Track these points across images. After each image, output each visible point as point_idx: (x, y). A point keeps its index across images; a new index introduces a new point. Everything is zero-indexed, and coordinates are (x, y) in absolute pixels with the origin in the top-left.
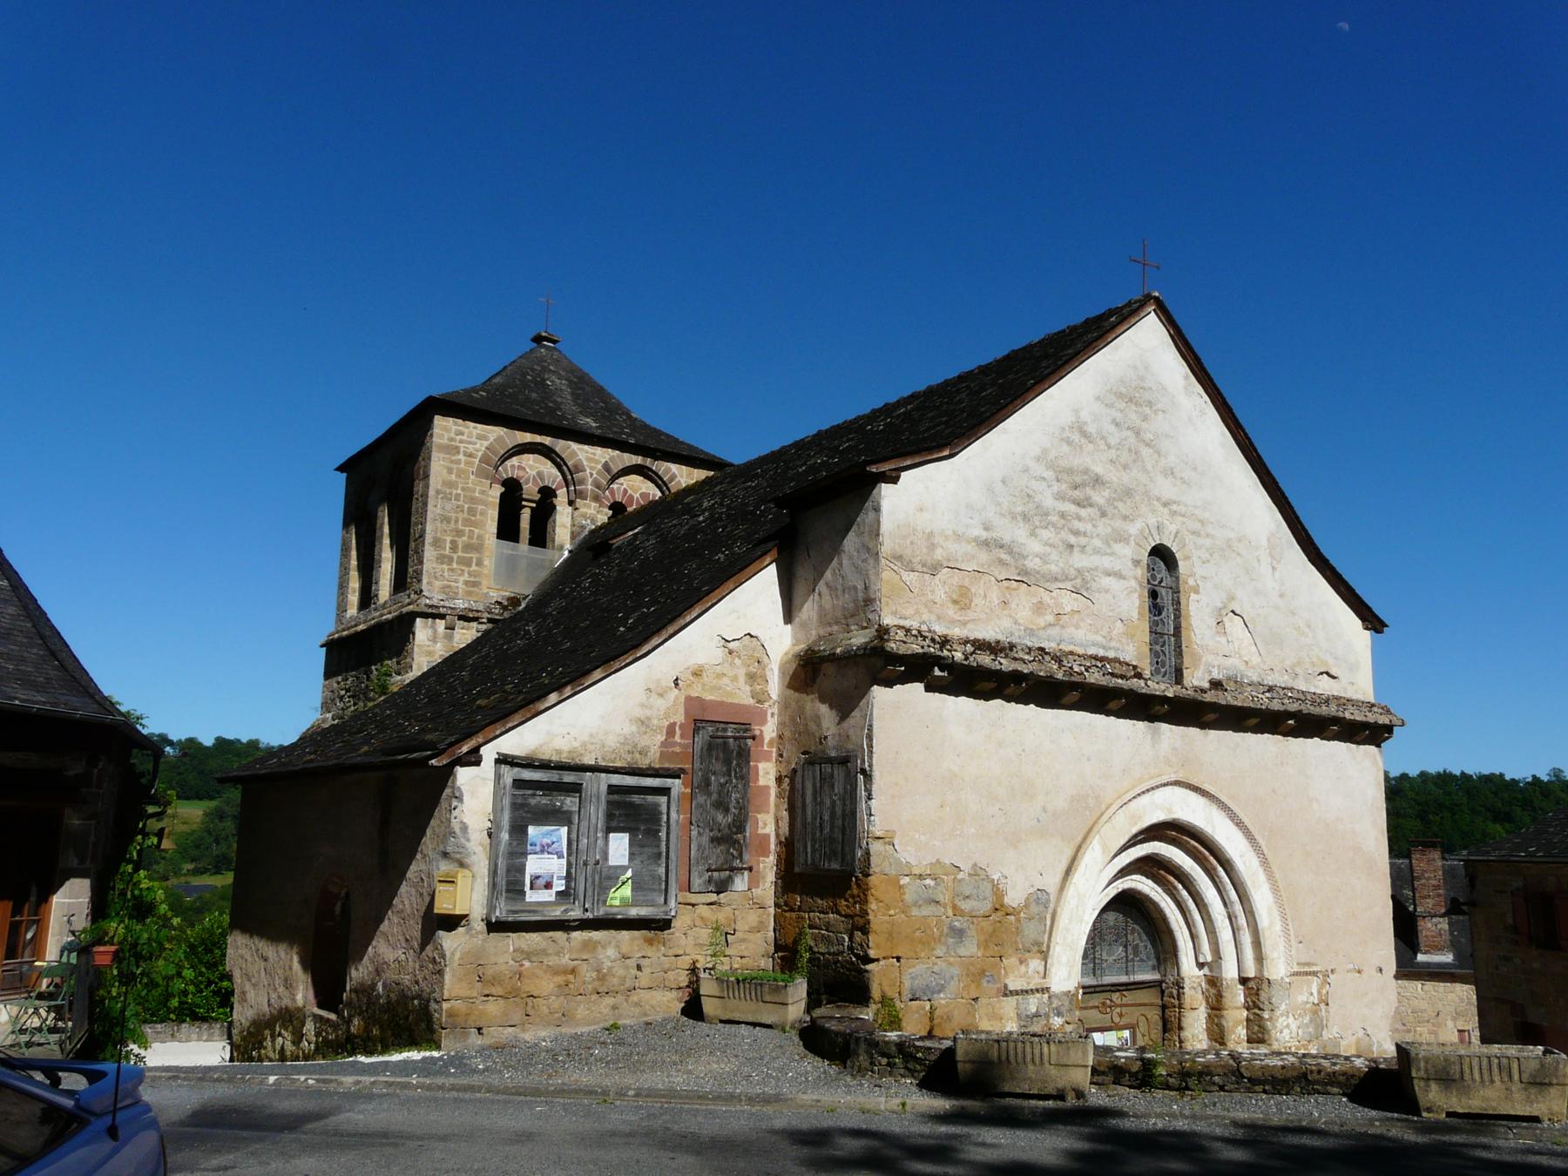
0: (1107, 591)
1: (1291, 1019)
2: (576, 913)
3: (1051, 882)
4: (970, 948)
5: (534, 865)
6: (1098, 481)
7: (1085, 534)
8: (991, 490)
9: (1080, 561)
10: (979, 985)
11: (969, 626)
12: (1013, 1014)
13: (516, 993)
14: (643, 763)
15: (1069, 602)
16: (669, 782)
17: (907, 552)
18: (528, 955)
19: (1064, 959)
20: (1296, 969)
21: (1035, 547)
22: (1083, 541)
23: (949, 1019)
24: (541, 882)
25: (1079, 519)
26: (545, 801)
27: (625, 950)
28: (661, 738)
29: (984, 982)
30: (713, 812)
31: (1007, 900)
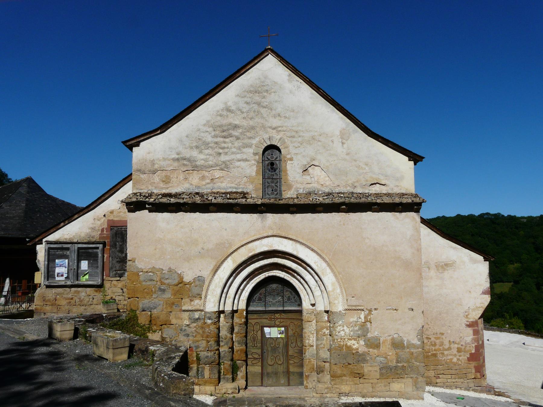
0: (238, 167)
1: (345, 328)
2: (69, 283)
3: (206, 274)
4: (168, 295)
5: (58, 270)
6: (236, 127)
7: (228, 148)
8: (181, 141)
9: (223, 158)
10: (172, 307)
11: (169, 189)
12: (187, 318)
13: (54, 303)
14: (93, 240)
15: (217, 174)
16: (98, 245)
17: (143, 168)
18: (58, 294)
19: (212, 300)
21: (200, 157)
22: (226, 150)
23: (158, 318)
24: (60, 275)
25: (225, 142)
26: (61, 253)
27: (88, 293)
28: (99, 232)
29: (174, 307)
30: (117, 253)
31: (184, 280)
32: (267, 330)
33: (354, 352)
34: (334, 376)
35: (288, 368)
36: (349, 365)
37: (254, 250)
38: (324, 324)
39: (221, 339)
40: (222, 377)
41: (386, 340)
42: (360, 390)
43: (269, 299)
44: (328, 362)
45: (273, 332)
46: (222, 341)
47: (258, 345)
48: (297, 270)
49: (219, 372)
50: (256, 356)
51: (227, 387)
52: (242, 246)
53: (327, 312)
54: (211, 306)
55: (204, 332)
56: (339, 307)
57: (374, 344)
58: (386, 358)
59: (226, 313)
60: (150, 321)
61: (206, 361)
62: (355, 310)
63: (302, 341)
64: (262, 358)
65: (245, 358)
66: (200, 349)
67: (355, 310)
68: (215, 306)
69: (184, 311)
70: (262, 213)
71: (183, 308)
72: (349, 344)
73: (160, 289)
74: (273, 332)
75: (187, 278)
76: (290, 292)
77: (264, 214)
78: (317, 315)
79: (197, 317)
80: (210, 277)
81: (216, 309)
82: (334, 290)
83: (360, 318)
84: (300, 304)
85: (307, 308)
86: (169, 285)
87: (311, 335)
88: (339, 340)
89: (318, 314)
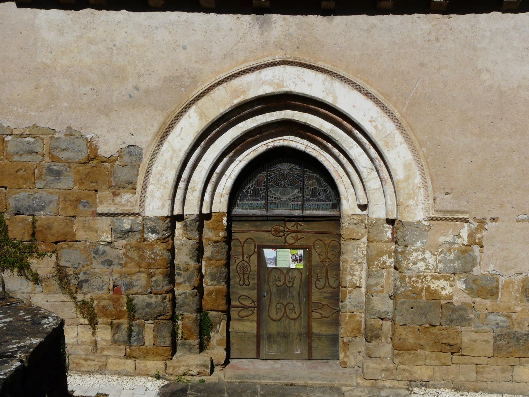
1: (428, 255)
3: (144, 140)
4: (67, 183)
10: (75, 207)
19: (158, 194)
20: (432, 214)
23: (49, 228)
29: (80, 207)
31: (99, 152)
32: (269, 253)
33: (443, 302)
34: (399, 348)
35: (309, 327)
36: (432, 327)
37: (244, 92)
38: (383, 246)
39: (177, 271)
40: (179, 342)
41: (512, 282)
42: (451, 377)
43: (275, 193)
44: (389, 319)
45: (279, 258)
46: (180, 275)
47: (252, 282)
48: (332, 135)
49: (174, 334)
50: (247, 303)
51: (189, 363)
52: (219, 83)
53: (391, 222)
54: (156, 206)
55: (141, 257)
56: (417, 212)
57: (486, 288)
58: (509, 317)
59: (188, 221)
60: (33, 234)
61: (147, 314)
62: (450, 219)
63: (338, 277)
64: (259, 307)
65: (224, 307)
66: (136, 289)
67: (450, 219)
68: (163, 206)
69: (102, 215)
70: (262, 14)
71: (99, 210)
72: (433, 287)
73: (50, 171)
74: (279, 258)
75: (106, 150)
76: (318, 181)
77: (266, 16)
78: (371, 227)
79: (127, 227)
80: (152, 148)
81: (166, 212)
82: (408, 178)
83: (460, 236)
84: (337, 205)
85: (351, 212)
86: (68, 163)
87: (357, 267)
88: (414, 279)
89: (373, 225)
